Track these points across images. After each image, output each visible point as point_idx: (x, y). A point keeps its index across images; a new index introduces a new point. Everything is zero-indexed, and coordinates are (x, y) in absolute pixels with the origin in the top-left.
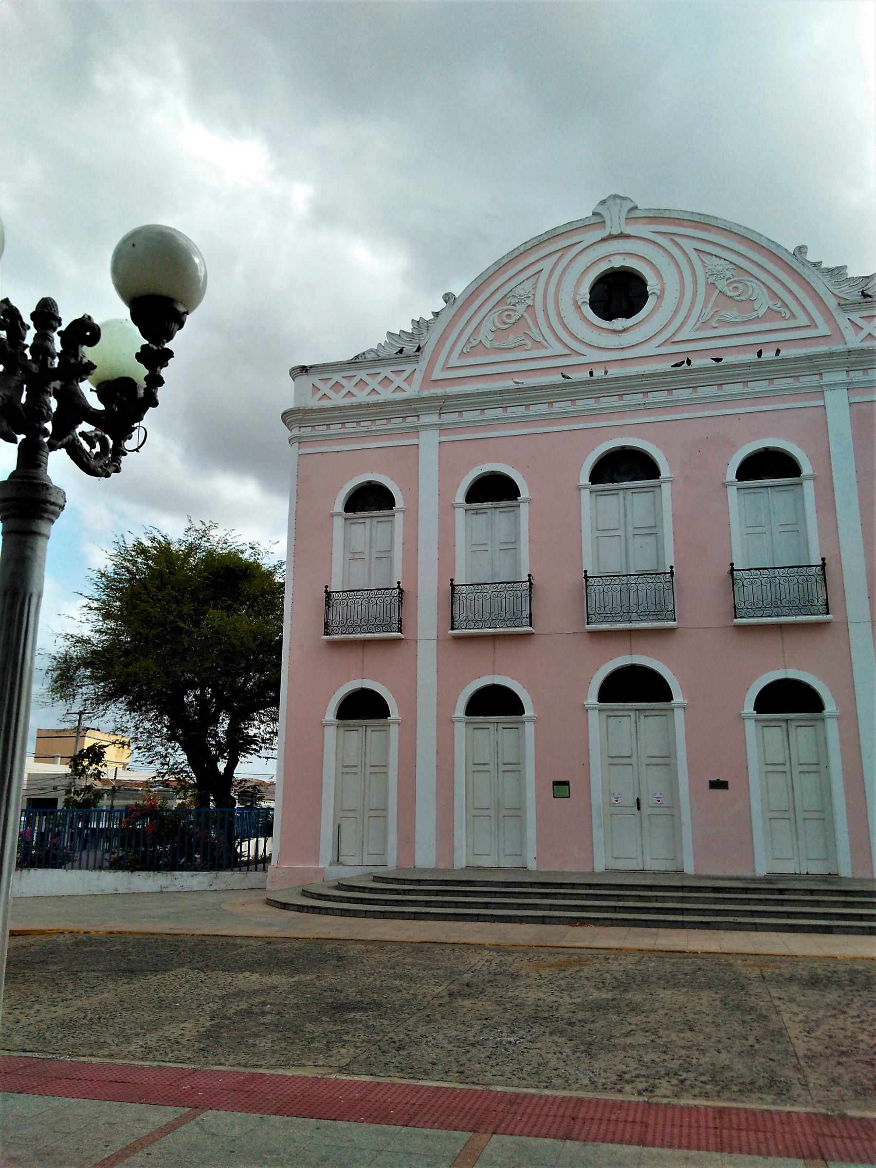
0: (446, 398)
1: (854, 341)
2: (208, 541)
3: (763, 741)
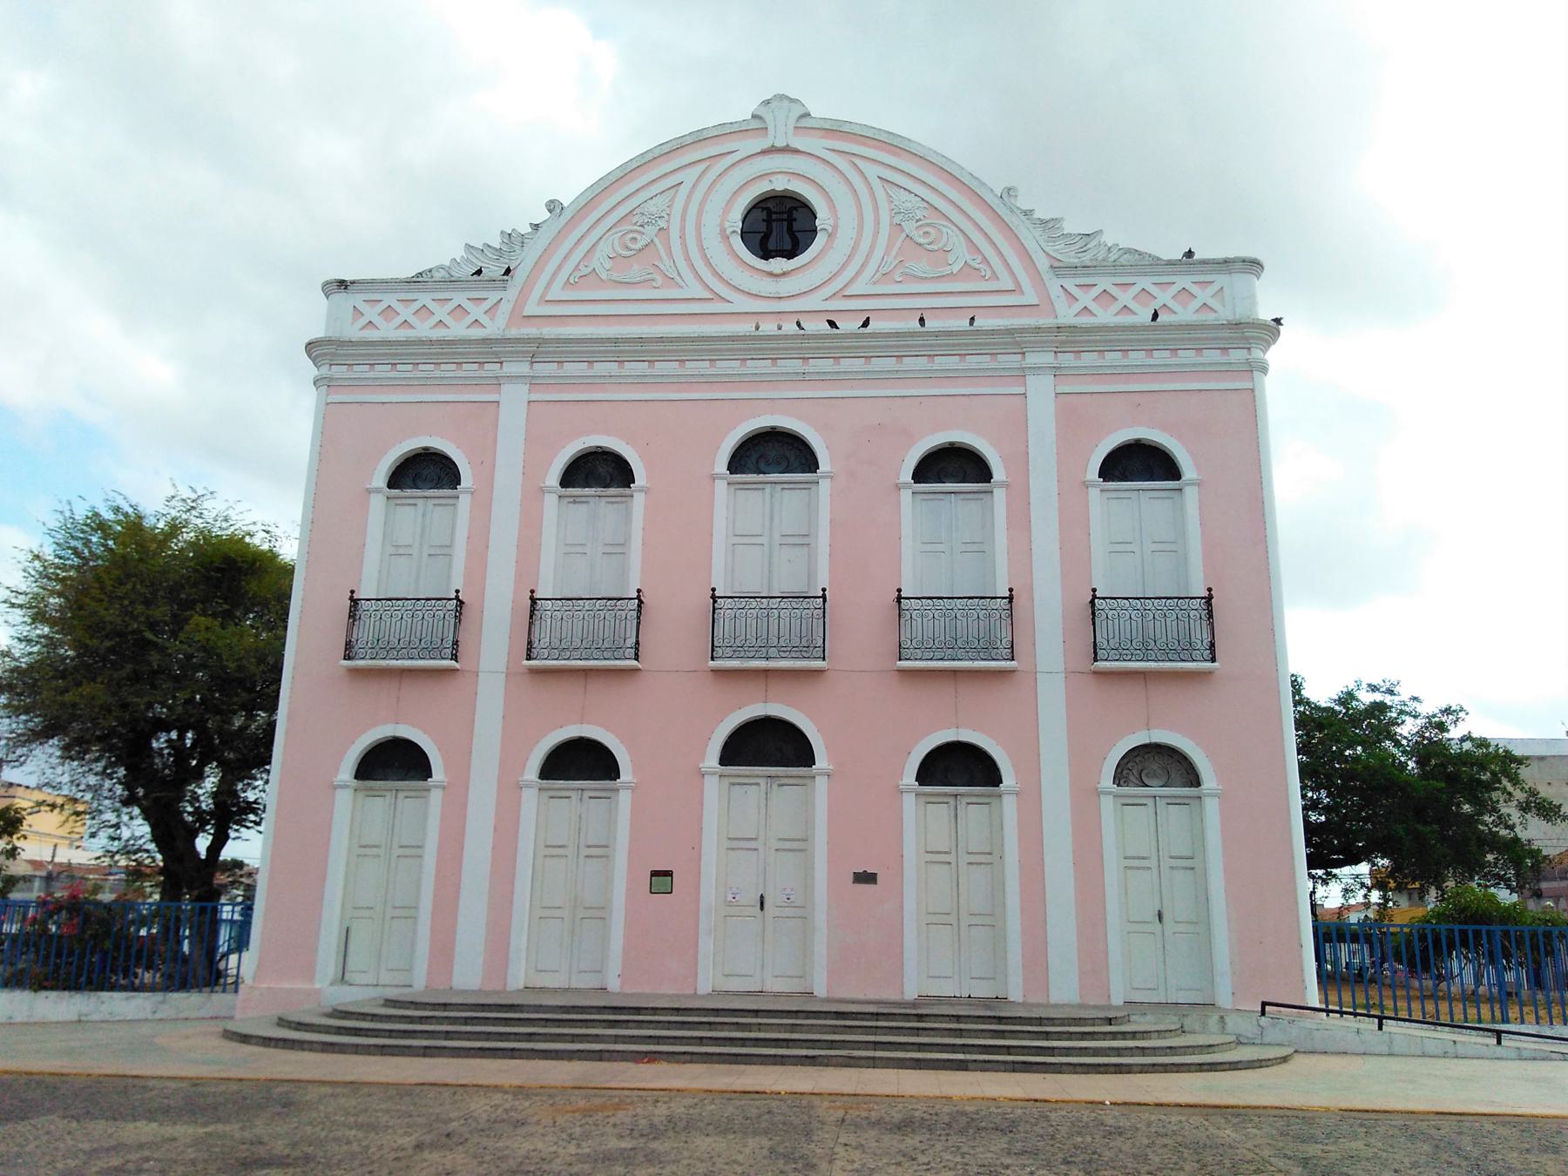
0: (541, 341)
1: (1067, 315)
2: (200, 516)
3: (925, 820)
